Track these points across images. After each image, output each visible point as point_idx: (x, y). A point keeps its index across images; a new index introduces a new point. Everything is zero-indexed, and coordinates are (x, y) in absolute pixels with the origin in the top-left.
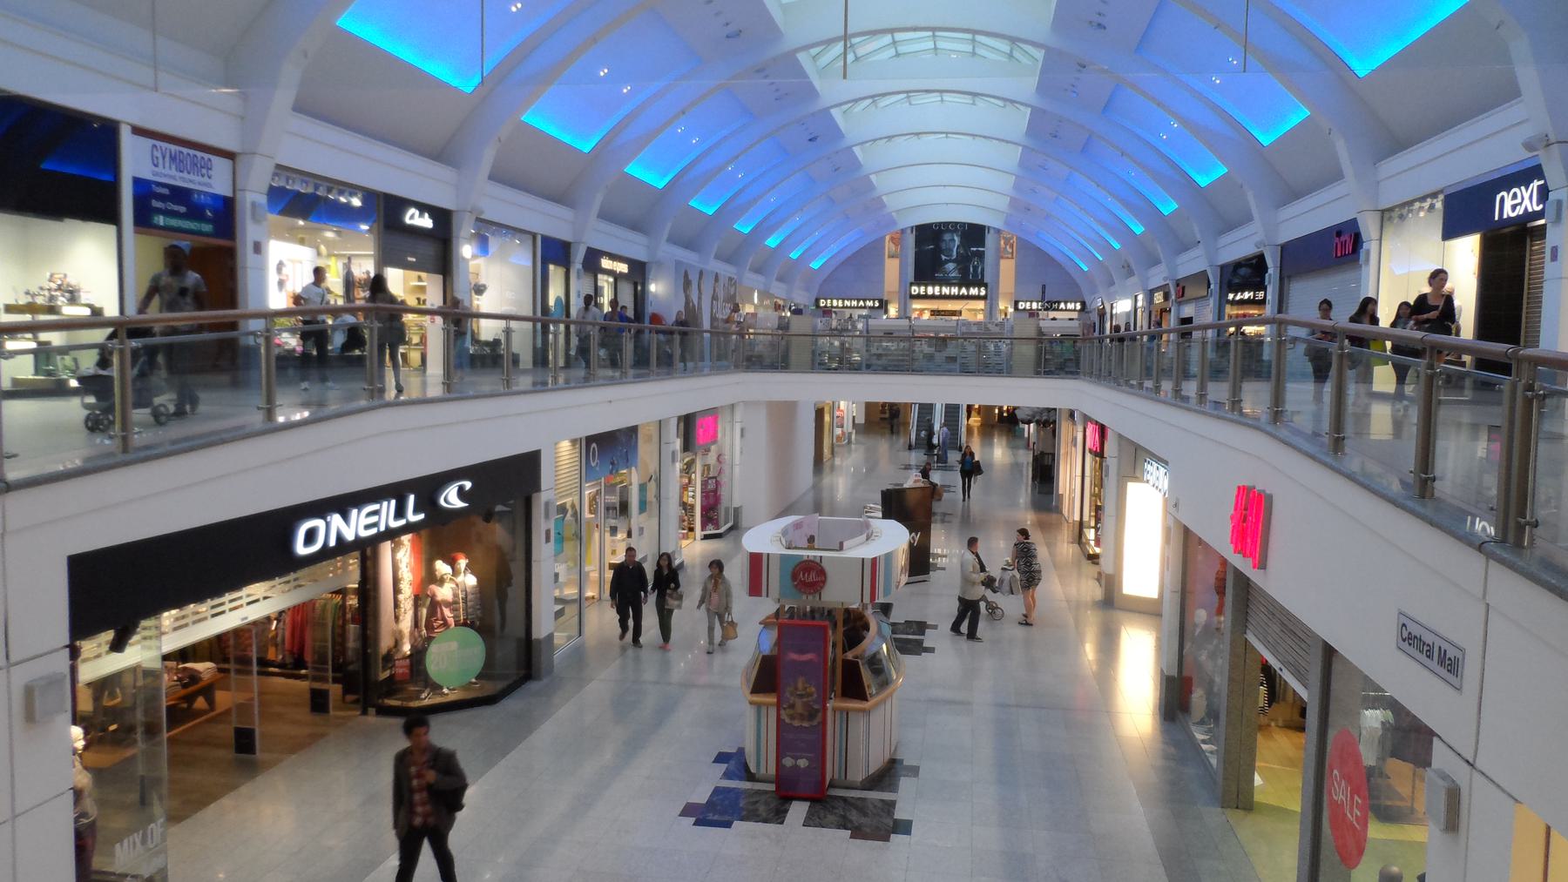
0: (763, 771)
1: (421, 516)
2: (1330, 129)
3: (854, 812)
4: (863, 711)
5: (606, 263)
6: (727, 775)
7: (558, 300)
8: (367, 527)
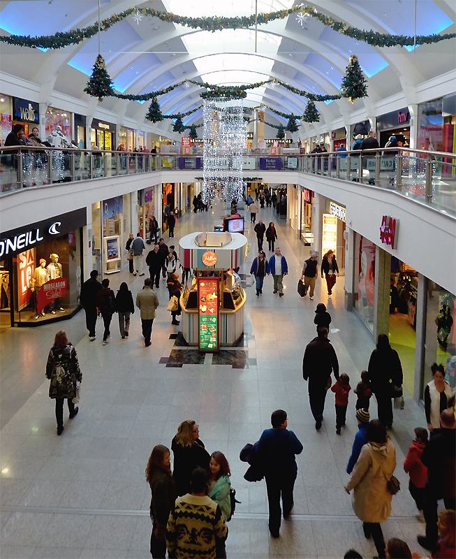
0: (192, 342)
1: (42, 238)
2: (143, 274)
3: (232, 356)
4: (233, 313)
5: (100, 125)
6: (176, 344)
7: (81, 141)
8: (20, 244)
